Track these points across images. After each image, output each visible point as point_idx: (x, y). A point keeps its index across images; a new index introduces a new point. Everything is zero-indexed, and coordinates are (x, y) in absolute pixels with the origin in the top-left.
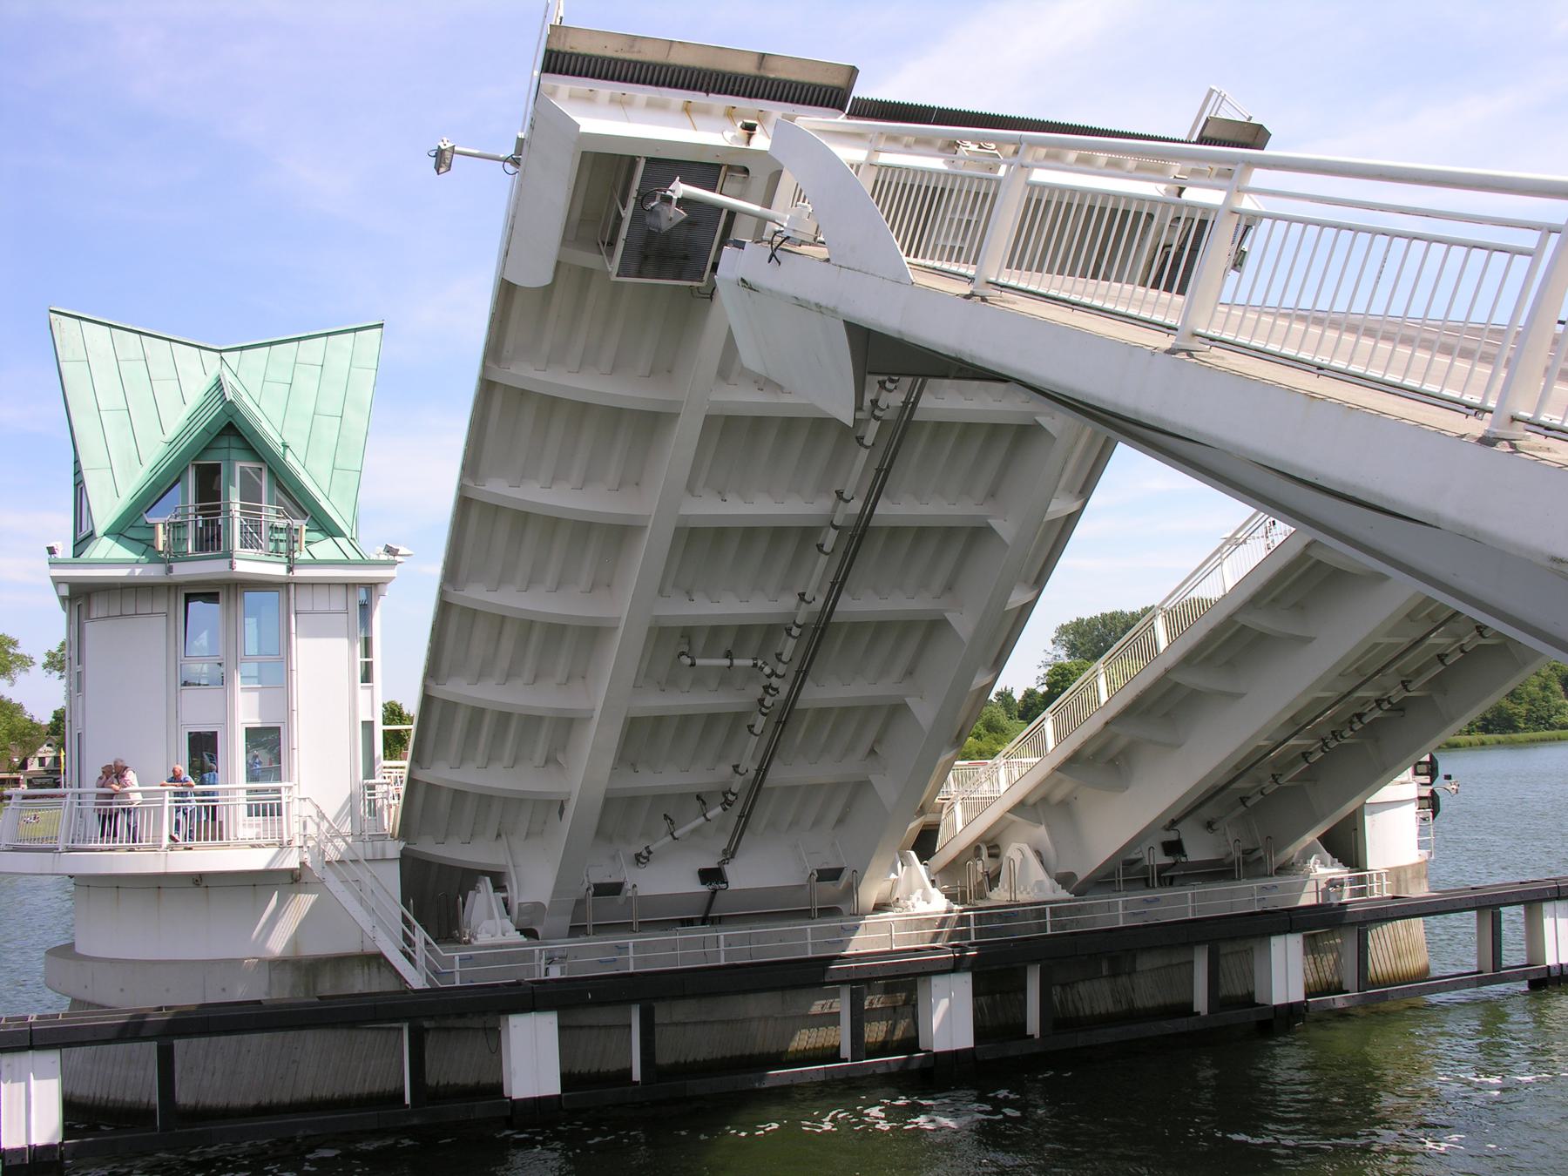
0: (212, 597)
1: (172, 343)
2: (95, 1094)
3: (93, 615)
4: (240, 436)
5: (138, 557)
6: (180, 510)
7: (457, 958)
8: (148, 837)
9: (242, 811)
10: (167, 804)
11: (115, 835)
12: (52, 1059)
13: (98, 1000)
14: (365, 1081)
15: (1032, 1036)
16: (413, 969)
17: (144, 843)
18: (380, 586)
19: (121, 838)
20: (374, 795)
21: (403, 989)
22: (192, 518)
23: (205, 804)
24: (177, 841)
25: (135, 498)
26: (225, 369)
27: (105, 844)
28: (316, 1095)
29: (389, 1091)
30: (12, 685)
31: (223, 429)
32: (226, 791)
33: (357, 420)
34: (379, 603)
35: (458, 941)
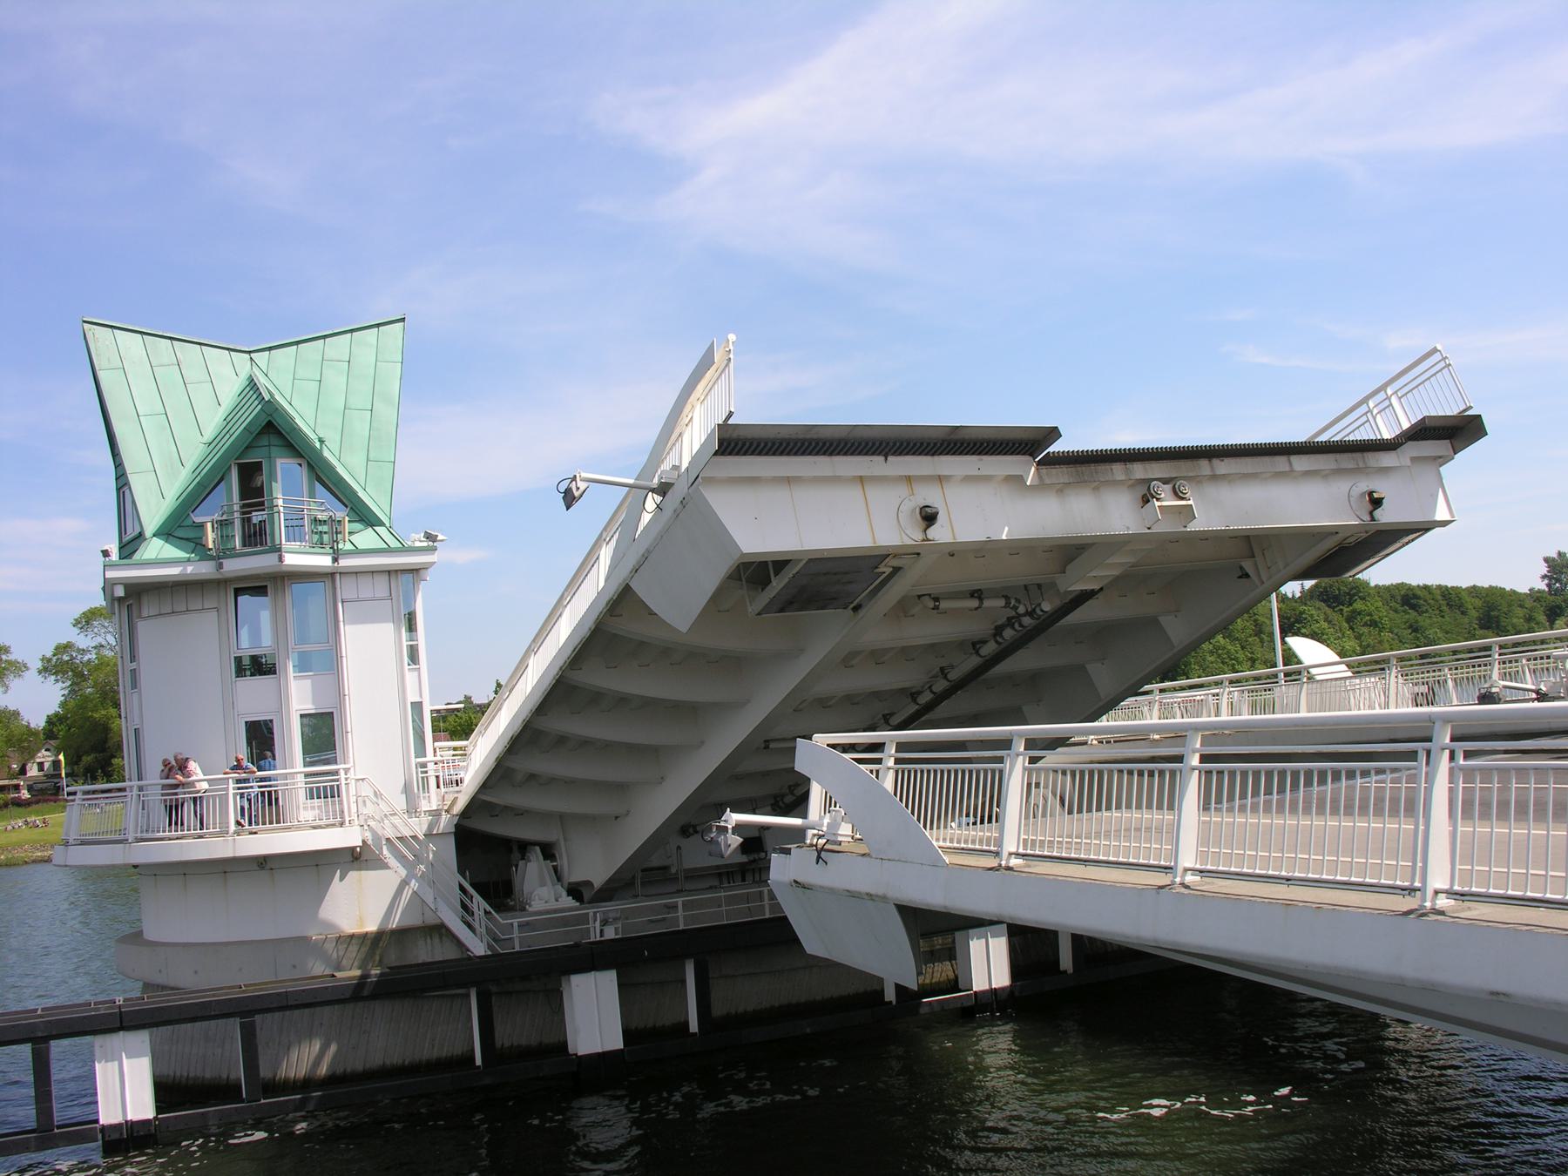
0: (260, 591)
1: (203, 347)
2: (175, 1073)
3: (145, 613)
4: (280, 434)
5: (188, 555)
6: (225, 508)
7: (516, 925)
8: (214, 824)
9: (302, 794)
10: (231, 792)
11: (182, 824)
12: (142, 1038)
13: (172, 984)
14: (433, 1046)
15: (1065, 972)
16: (473, 935)
17: (211, 830)
18: (421, 571)
19: (189, 826)
20: (426, 772)
21: (465, 956)
22: (237, 515)
23: (268, 789)
24: (243, 826)
25: (181, 498)
26: (255, 369)
27: (173, 833)
28: (388, 1062)
29: (457, 1056)
30: (6, 692)
31: (263, 428)
32: (285, 776)
33: (387, 413)
34: (420, 586)
35: (512, 909)
